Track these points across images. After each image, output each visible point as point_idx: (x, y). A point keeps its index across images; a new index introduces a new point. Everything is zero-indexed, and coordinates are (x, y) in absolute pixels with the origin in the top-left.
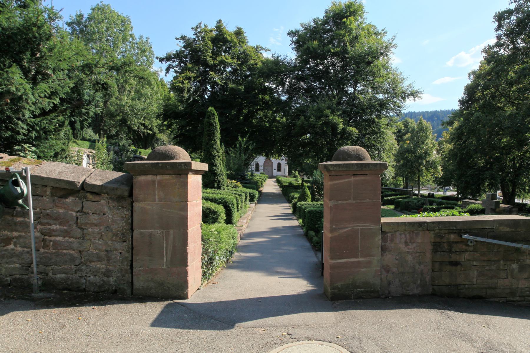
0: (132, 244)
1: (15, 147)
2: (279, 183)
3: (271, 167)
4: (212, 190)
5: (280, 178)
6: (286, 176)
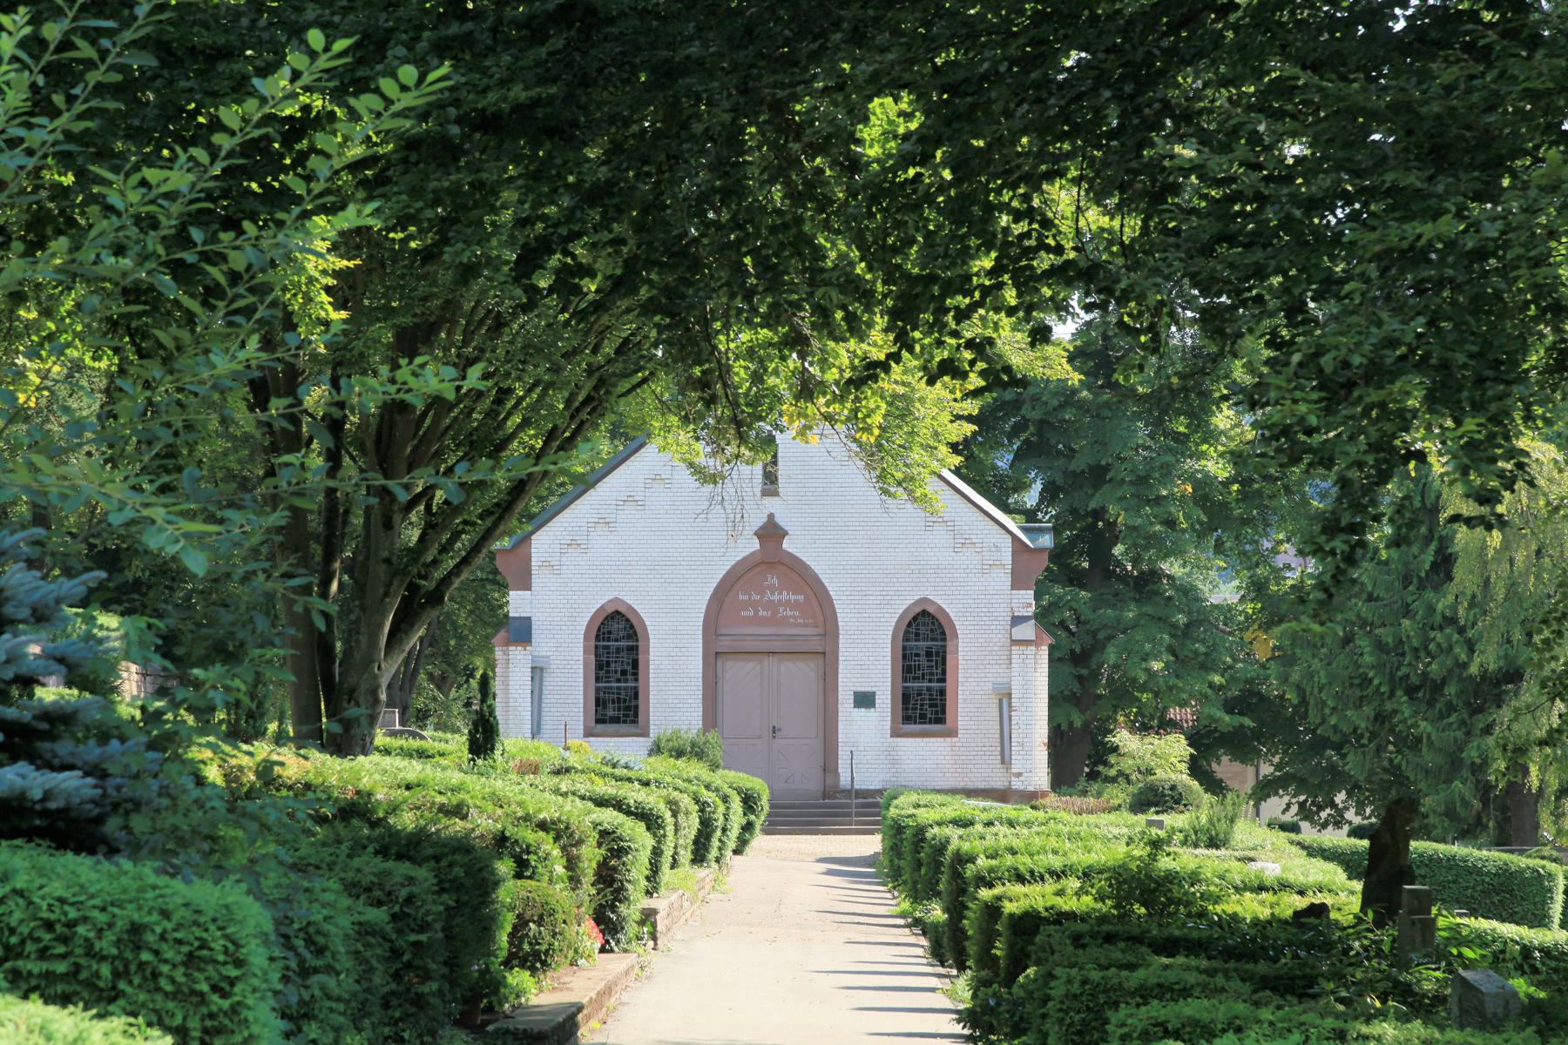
0: (953, 792)
1: (1252, 725)
2: (920, 892)
3: (801, 673)
4: (740, 811)
5: (932, 814)
6: (1030, 798)
